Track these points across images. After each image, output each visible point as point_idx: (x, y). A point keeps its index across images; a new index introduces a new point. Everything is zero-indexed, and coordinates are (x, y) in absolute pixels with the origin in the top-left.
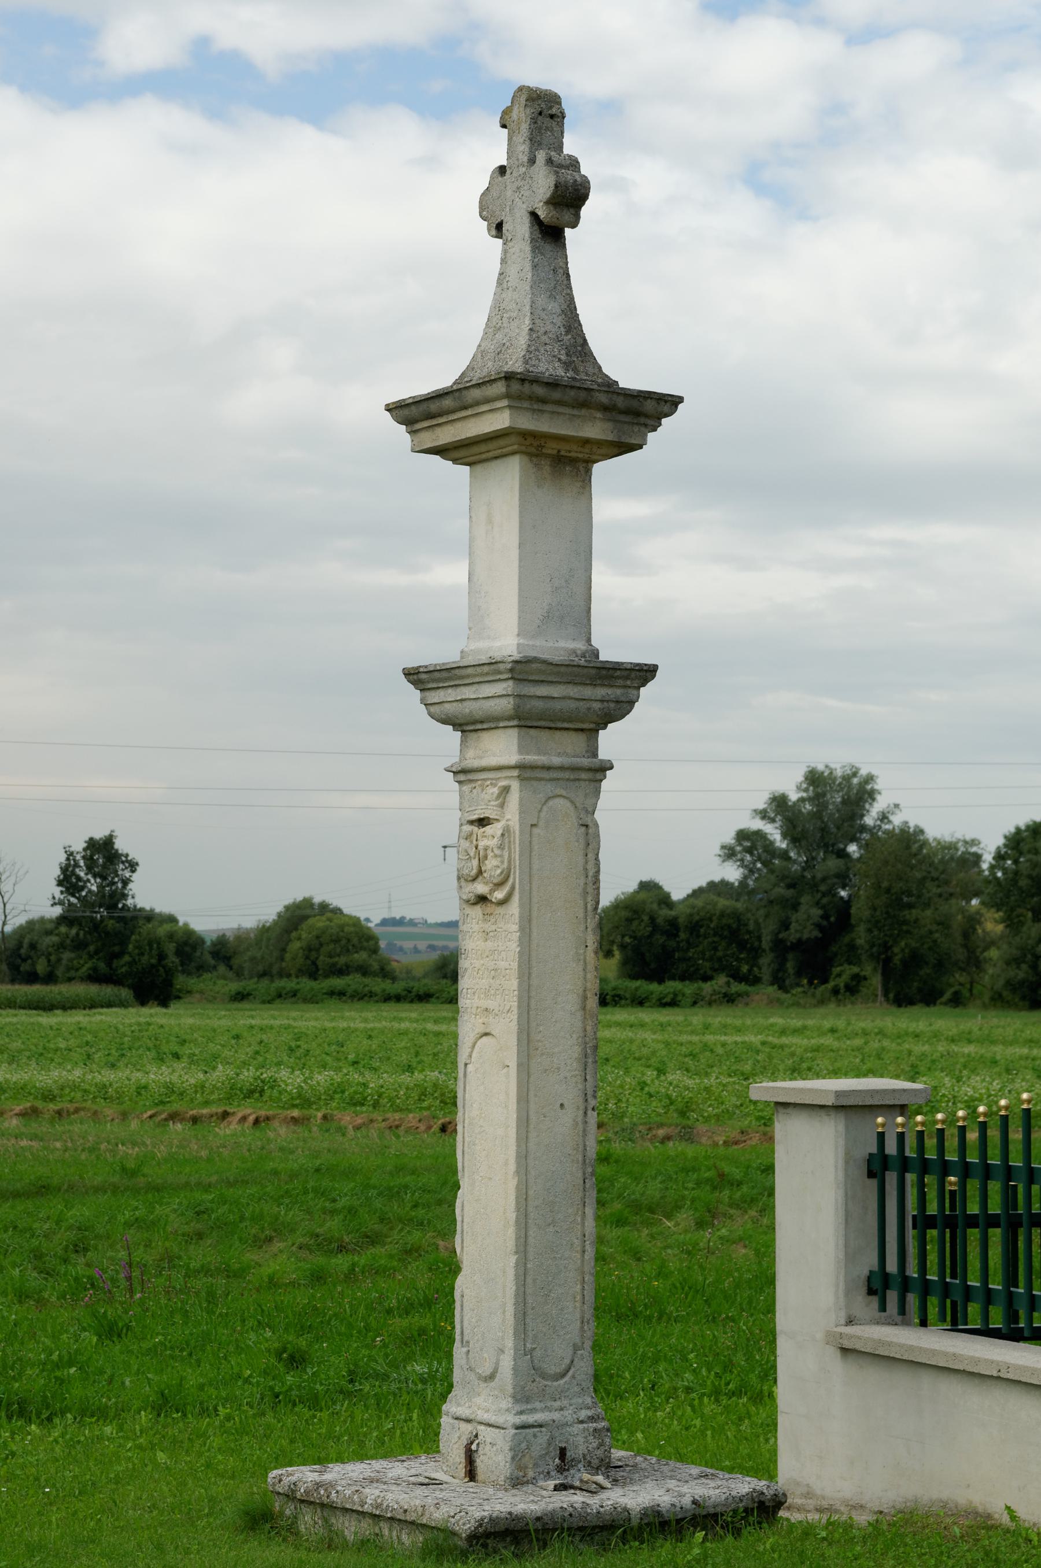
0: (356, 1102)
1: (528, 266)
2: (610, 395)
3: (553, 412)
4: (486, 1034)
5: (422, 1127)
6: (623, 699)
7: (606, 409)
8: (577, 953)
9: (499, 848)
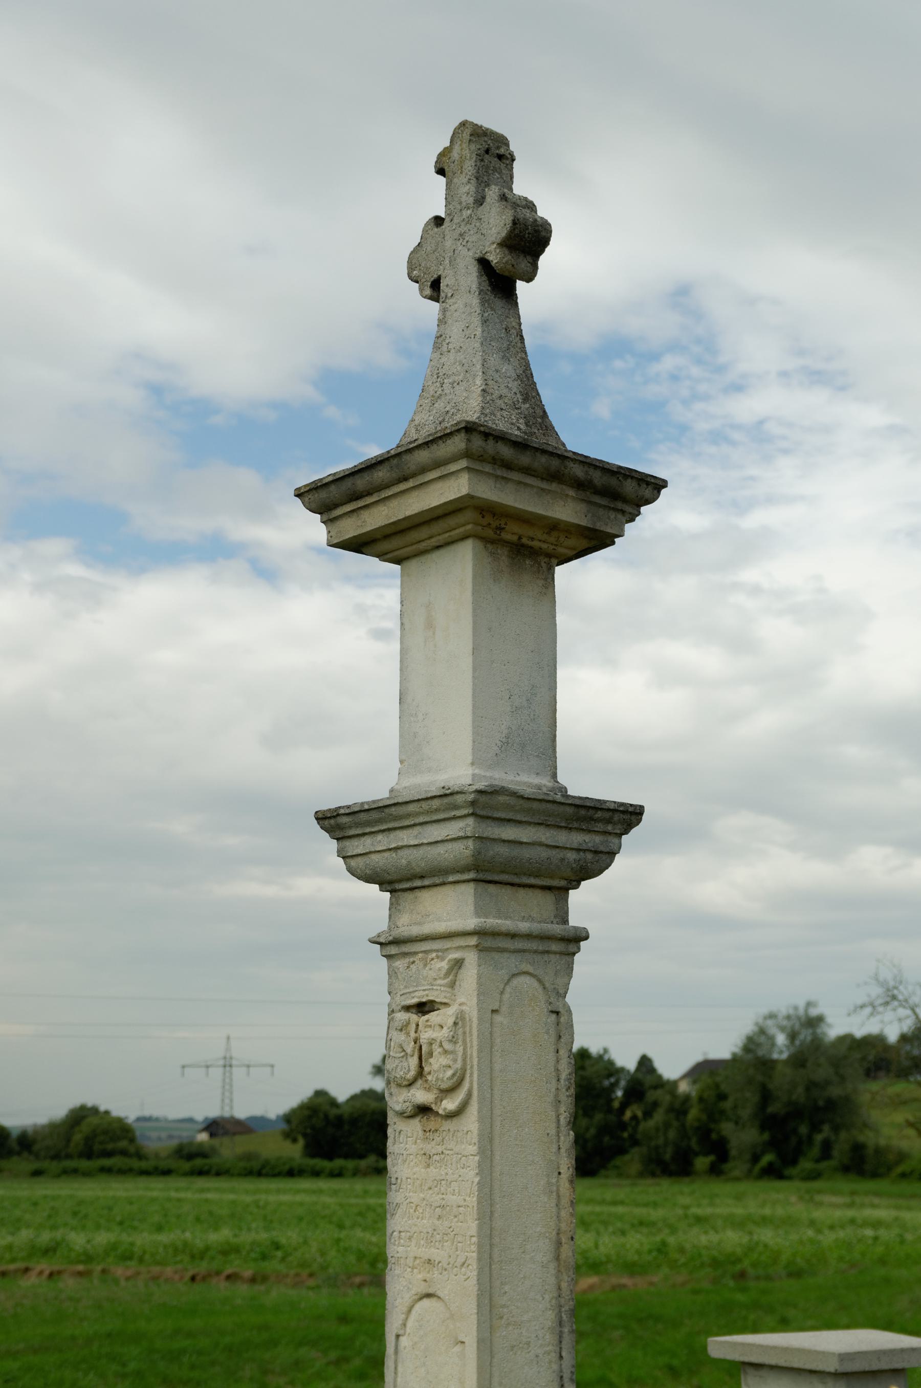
0: (127, 1257)
1: (476, 321)
2: (586, 468)
3: (520, 483)
4: (429, 1296)
5: (177, 1277)
6: (602, 848)
7: (580, 485)
8: (549, 1183)
9: (450, 1041)
